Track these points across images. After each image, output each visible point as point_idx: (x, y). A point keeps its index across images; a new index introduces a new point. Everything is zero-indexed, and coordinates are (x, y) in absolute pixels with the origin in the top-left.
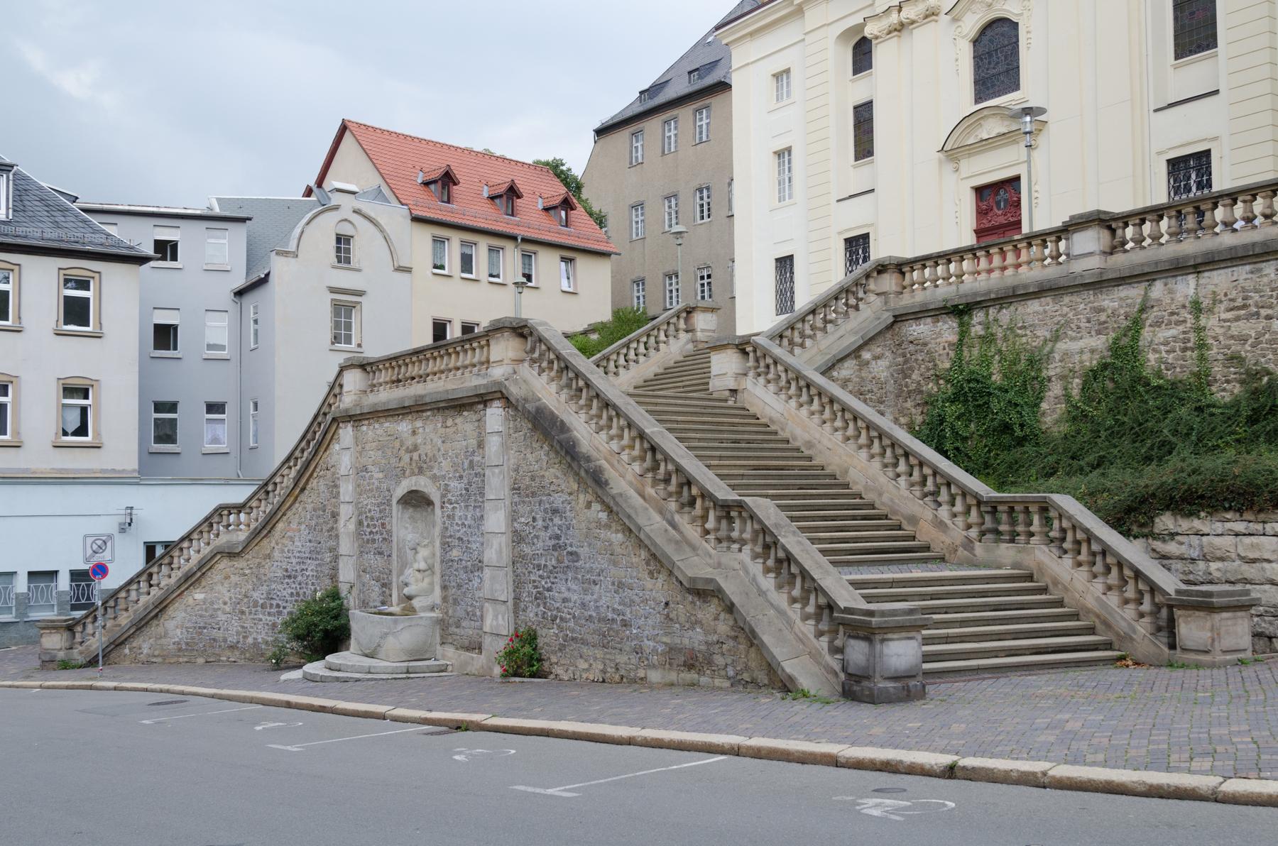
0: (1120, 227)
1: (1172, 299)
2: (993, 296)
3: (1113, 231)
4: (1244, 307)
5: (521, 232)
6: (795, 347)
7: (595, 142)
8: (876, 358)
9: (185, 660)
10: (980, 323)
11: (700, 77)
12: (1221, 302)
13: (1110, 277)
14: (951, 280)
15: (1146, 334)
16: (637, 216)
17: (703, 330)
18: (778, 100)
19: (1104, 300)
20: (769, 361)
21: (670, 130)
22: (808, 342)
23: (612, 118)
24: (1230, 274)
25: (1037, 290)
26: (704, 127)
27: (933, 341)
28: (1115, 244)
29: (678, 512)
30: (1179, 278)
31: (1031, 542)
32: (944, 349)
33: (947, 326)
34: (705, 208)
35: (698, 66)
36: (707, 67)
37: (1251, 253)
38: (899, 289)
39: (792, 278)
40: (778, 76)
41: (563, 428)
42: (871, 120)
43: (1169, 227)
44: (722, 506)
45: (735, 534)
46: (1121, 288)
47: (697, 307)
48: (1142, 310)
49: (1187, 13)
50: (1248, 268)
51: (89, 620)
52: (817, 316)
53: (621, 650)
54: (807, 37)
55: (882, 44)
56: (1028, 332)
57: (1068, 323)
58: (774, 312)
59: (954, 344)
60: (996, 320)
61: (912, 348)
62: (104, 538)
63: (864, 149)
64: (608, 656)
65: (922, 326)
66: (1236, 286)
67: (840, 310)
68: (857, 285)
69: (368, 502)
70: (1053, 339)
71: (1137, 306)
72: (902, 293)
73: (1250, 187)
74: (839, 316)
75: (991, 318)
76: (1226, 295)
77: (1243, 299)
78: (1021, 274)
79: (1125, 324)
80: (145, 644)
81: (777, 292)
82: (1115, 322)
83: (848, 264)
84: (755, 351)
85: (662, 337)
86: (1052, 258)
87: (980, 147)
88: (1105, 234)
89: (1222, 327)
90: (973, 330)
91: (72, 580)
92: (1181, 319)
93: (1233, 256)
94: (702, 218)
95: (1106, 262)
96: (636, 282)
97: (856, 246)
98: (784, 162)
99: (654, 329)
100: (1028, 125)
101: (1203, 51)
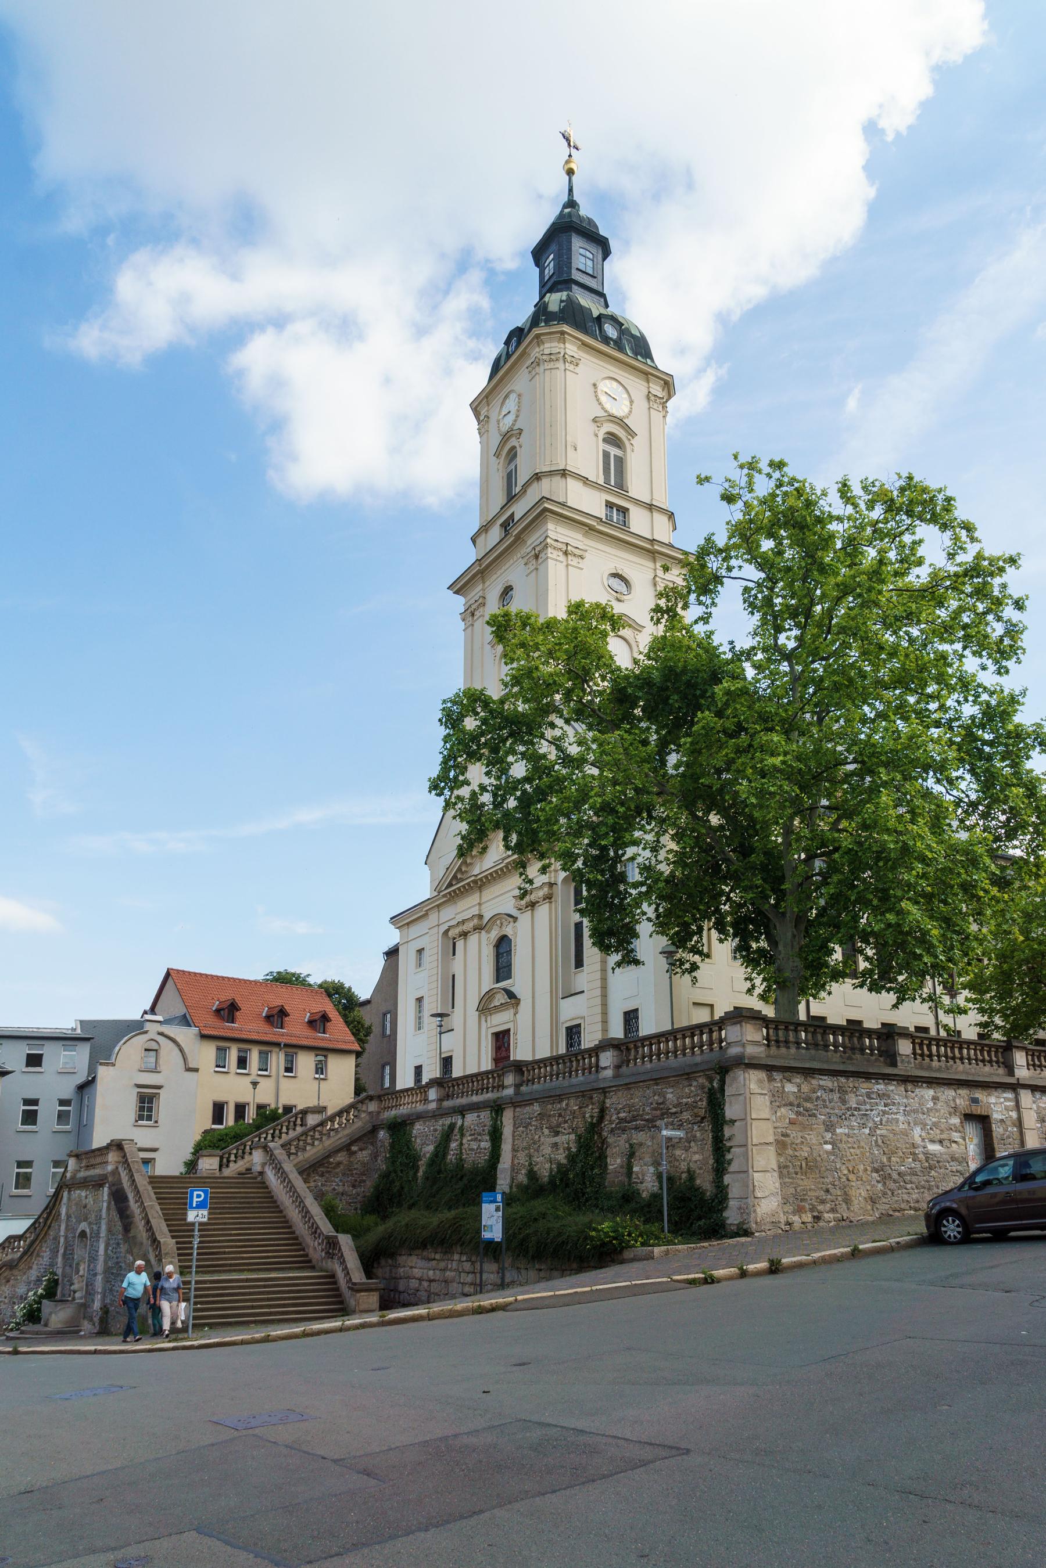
5: (283, 1040)
8: (361, 1150)
22: (316, 1143)
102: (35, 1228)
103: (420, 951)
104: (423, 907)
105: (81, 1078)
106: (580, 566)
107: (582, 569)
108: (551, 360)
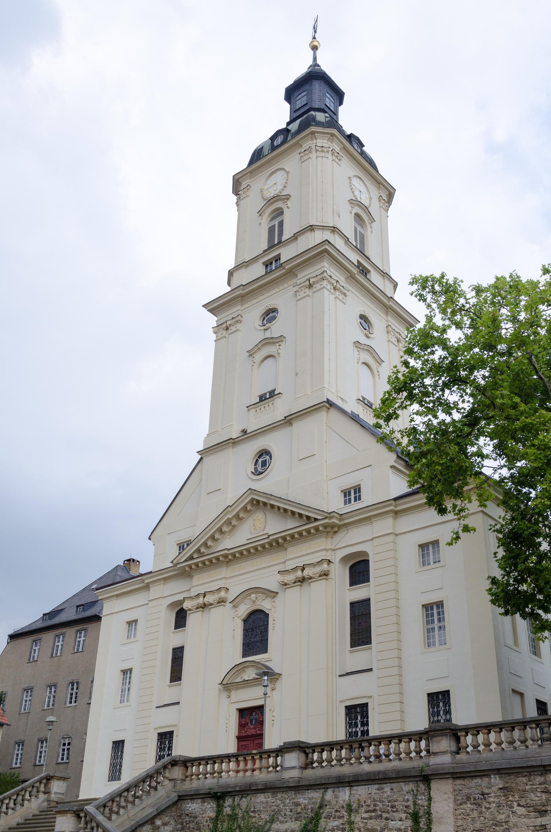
0: (310, 753)
1: (337, 802)
2: (238, 789)
3: (307, 754)
4: (374, 811)
6: (113, 814)
7: (8, 643)
8: (165, 824)
10: (229, 806)
11: (84, 610)
12: (362, 806)
13: (303, 784)
14: (215, 775)
15: (322, 822)
16: (27, 696)
17: (56, 793)
18: (128, 638)
19: (300, 798)
20: (94, 824)
21: (59, 642)
22: (122, 811)
23: (22, 629)
24: (367, 789)
25: (263, 788)
26: (82, 642)
27: (200, 815)
28: (307, 762)
30: (341, 789)
32: (207, 822)
33: (210, 806)
34: (74, 696)
35: (83, 603)
36: (89, 604)
37: (377, 778)
38: (183, 778)
39: (122, 755)
40: (130, 623)
42: (182, 658)
43: (336, 756)
46: (309, 791)
47: (54, 776)
48: (321, 807)
49: (357, 622)
50: (376, 786)
52: (130, 793)
54: (150, 603)
55: (192, 614)
56: (257, 815)
57: (279, 811)
58: (107, 778)
59: (213, 819)
60: (239, 805)
61: (187, 819)
63: (176, 676)
65: (195, 804)
66: (370, 797)
67: (145, 790)
68: (157, 773)
70: (271, 821)
71: (318, 804)
72: (185, 780)
74: (144, 794)
75: (236, 803)
76: (365, 802)
77: (374, 806)
78: (255, 775)
79: (311, 815)
81: (111, 764)
82: (306, 813)
83: (158, 751)
84: (85, 817)
85: (27, 796)
86: (273, 767)
87: (241, 685)
88: (303, 756)
89: (363, 822)
90: (225, 810)
92: (341, 815)
93: (368, 778)
94: (71, 702)
95: (302, 773)
96: (18, 743)
97: (164, 739)
98: (126, 677)
99: (22, 790)
100: (266, 681)
101: (365, 645)
103: (133, 623)
106: (344, 301)
107: (345, 304)
108: (322, 151)
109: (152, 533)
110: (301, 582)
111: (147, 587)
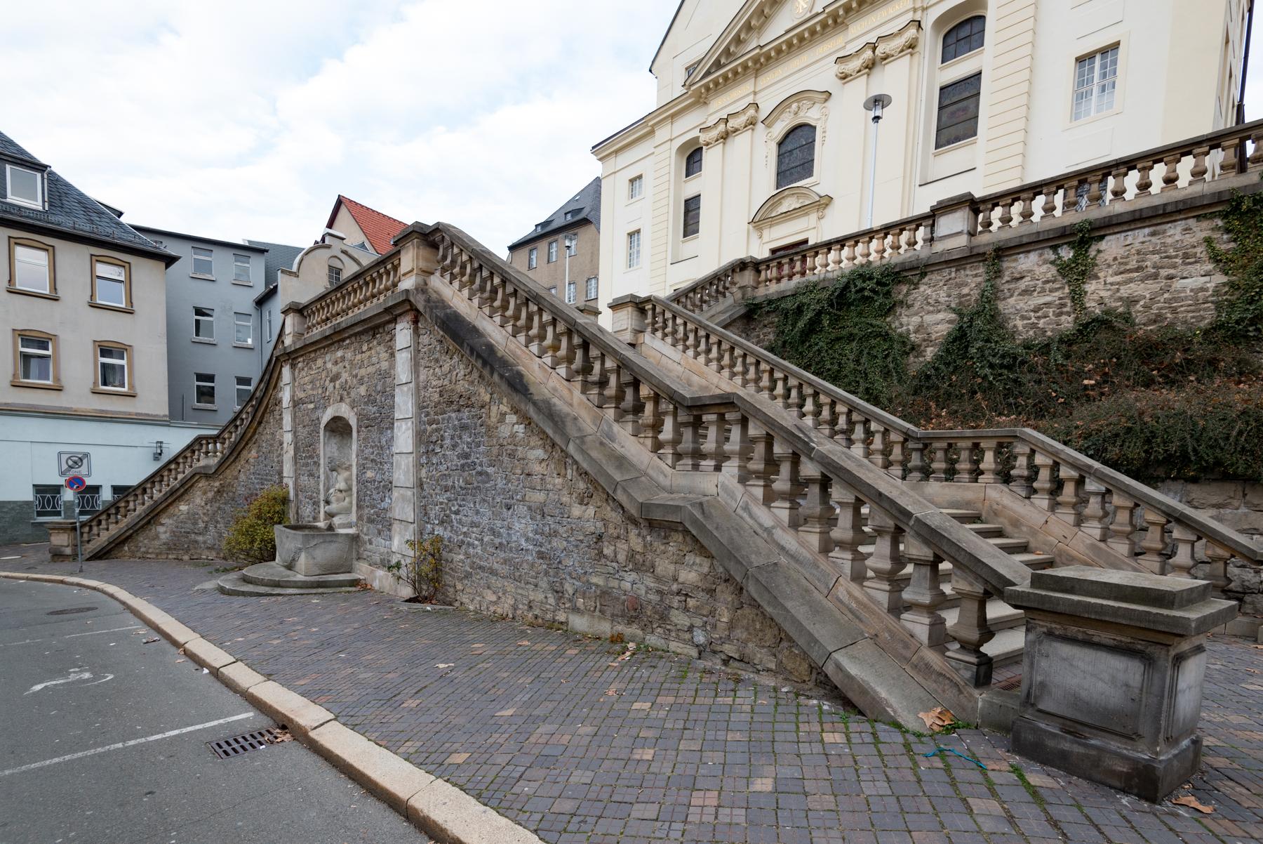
9: (174, 557)
29: (617, 421)
31: (979, 481)
41: (475, 330)
44: (689, 408)
45: (709, 445)
50: (1147, 231)
51: (94, 523)
53: (536, 586)
62: (80, 456)
64: (520, 591)
69: (303, 432)
73: (1161, 150)
80: (143, 541)
91: (114, 493)
102: (237, 427)
104: (650, 120)
105: (260, 289)
109: (653, 62)
110: (870, 69)
111: (652, 132)
